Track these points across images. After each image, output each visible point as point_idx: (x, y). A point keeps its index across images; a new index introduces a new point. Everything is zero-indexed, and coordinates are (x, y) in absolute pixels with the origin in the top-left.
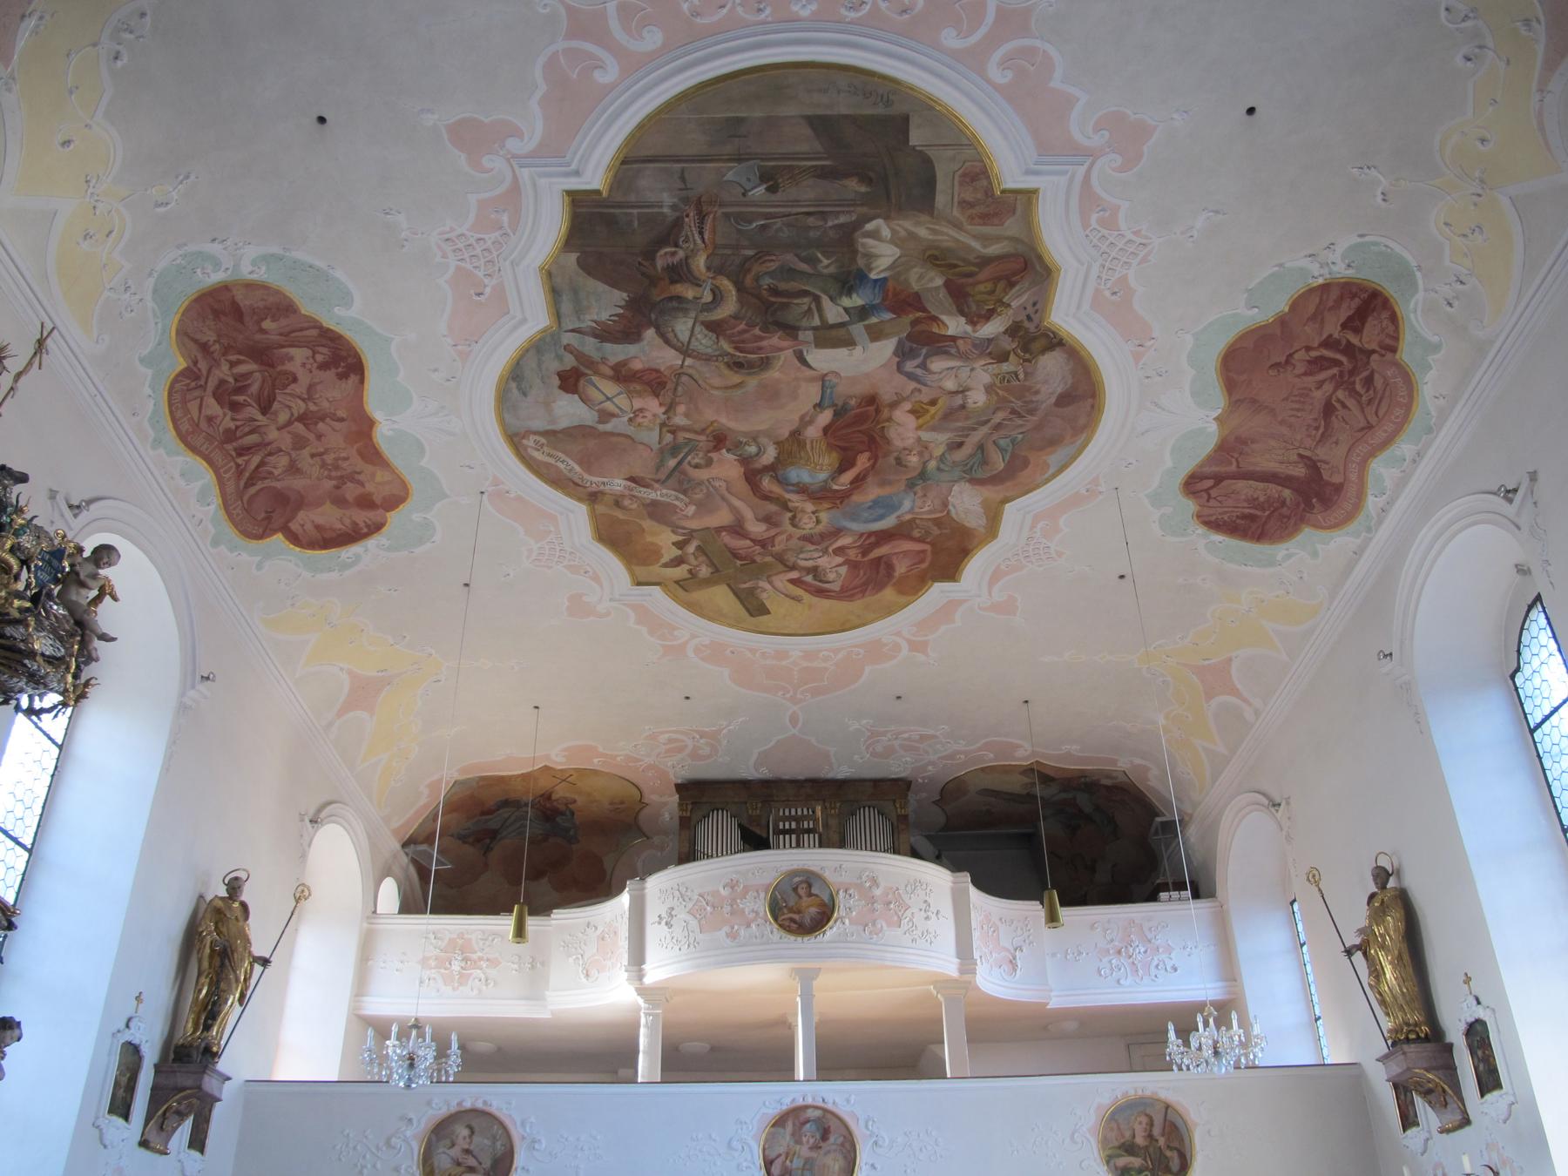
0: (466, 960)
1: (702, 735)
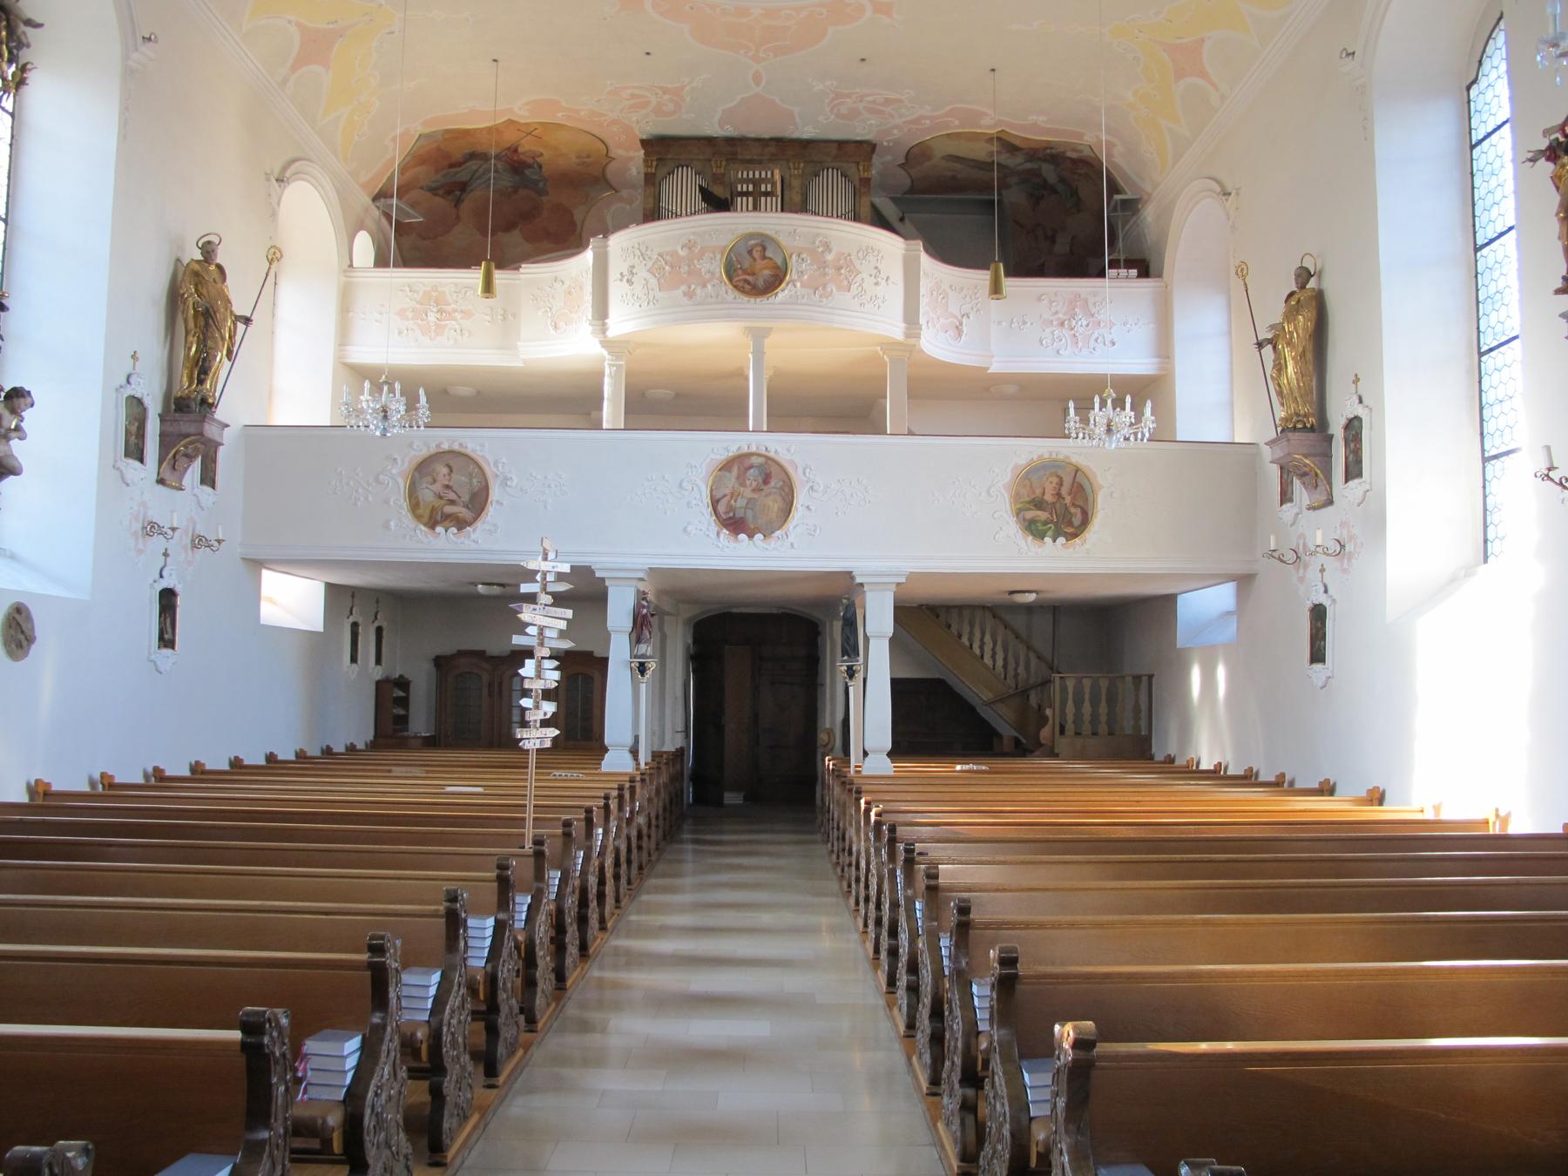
0: (440, 311)
1: (665, 91)
